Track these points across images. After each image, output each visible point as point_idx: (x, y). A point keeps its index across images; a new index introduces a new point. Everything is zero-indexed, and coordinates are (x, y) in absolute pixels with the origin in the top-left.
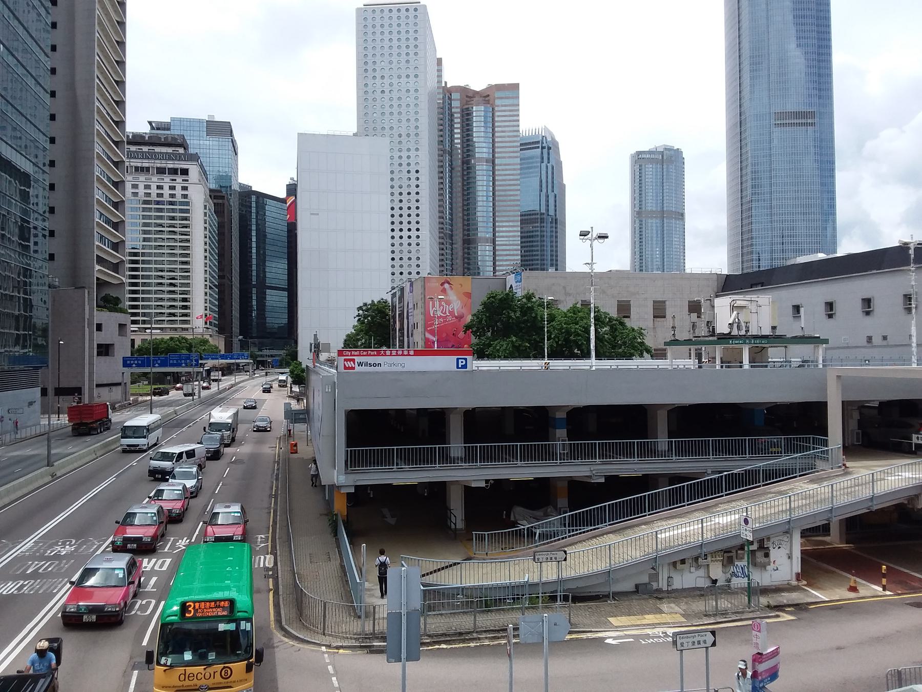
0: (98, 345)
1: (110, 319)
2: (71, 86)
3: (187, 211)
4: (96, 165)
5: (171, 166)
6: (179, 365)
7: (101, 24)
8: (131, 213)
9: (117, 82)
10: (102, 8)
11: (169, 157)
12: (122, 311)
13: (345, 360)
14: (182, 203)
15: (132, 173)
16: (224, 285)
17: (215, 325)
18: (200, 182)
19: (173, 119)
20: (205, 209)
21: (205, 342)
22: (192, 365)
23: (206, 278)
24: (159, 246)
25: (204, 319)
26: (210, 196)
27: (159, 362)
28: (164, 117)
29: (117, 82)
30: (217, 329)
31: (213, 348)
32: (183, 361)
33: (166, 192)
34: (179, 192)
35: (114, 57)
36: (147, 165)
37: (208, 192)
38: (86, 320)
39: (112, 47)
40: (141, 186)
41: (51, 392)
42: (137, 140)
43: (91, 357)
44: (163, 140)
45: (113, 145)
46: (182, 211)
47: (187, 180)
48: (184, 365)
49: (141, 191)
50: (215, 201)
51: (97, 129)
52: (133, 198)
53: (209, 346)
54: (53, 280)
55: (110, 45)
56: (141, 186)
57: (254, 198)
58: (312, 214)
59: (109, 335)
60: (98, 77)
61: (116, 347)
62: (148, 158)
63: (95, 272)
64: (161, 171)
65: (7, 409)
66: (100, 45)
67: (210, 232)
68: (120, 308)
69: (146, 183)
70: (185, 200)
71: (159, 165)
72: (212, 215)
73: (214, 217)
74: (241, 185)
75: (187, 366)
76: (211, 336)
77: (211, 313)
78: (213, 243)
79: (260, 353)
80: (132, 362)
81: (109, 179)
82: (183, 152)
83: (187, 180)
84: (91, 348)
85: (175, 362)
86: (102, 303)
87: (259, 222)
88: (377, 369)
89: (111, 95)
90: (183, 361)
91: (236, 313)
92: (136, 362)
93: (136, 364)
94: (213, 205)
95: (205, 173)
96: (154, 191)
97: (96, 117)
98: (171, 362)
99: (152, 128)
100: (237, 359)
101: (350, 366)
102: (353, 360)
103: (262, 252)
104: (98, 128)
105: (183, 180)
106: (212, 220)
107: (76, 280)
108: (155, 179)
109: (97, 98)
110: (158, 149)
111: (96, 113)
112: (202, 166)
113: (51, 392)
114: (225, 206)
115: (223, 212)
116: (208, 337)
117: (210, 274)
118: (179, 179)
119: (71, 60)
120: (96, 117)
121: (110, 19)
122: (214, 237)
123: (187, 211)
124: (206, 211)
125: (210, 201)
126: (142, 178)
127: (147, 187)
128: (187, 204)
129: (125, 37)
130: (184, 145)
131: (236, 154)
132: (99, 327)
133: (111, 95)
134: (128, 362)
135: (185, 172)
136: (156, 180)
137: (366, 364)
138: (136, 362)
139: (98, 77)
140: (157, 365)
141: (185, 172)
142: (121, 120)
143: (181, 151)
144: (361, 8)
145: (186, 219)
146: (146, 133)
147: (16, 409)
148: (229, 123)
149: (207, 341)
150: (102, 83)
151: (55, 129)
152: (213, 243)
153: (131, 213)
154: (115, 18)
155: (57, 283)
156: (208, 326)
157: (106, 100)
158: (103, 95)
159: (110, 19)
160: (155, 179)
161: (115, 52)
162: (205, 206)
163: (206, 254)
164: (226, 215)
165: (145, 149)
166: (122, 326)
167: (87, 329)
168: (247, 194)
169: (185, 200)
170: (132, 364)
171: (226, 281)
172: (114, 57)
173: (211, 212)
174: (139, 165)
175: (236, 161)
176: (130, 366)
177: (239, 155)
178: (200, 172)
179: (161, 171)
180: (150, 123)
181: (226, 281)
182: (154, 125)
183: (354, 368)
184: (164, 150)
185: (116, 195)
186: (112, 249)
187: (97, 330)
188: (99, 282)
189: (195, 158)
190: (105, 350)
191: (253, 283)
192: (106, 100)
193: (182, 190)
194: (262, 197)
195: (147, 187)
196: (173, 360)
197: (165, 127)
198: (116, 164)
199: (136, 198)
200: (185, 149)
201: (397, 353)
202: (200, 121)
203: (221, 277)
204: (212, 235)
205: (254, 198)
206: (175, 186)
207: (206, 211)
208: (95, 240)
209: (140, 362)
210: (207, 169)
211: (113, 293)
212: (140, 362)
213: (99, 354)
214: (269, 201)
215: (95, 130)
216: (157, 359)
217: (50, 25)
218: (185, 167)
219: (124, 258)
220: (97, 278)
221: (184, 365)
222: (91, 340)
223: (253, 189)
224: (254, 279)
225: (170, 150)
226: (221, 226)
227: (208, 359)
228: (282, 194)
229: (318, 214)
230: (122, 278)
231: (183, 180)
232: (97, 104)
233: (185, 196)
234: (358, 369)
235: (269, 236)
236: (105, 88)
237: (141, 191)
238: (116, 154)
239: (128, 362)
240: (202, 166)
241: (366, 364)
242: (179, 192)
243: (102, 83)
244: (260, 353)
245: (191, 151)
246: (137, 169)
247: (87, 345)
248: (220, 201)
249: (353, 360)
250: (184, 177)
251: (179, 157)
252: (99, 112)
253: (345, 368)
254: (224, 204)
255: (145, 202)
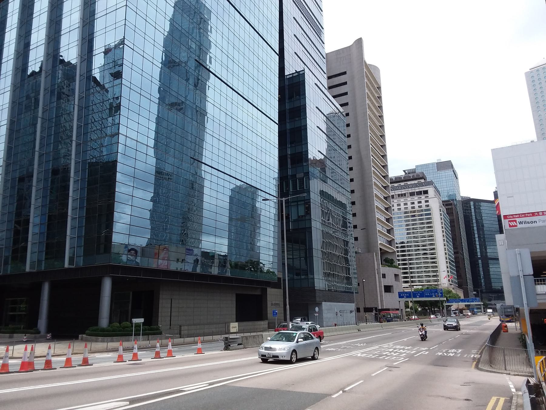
0: (385, 286)
1: (389, 271)
2: (359, 152)
3: (430, 214)
4: (376, 212)
5: (418, 190)
6: (431, 296)
7: (370, 118)
8: (398, 224)
9: (381, 146)
10: (371, 111)
11: (416, 186)
12: (395, 267)
13: (509, 221)
14: (426, 210)
15: (396, 198)
16: (458, 258)
17: (455, 283)
18: (435, 196)
19: (417, 166)
20: (441, 211)
21: (449, 292)
22: (438, 296)
23: (446, 257)
24: (418, 254)
25: (448, 278)
26: (443, 205)
27: (419, 294)
28: (412, 166)
29: (381, 146)
30: (457, 285)
31: (456, 295)
32: (433, 294)
33: (416, 205)
34: (423, 204)
35: (379, 134)
36: (403, 193)
37: (442, 202)
38: (376, 270)
39: (378, 139)
40: (402, 204)
41: (362, 310)
42: (398, 180)
43: (381, 292)
44: (412, 177)
45: (382, 168)
46: (426, 215)
47: (428, 197)
48: (434, 296)
49: (402, 207)
50: (447, 207)
51: (373, 170)
52: (398, 211)
53: (452, 294)
54: (358, 250)
55: (377, 120)
56: (402, 204)
57: (472, 203)
58: (508, 197)
59: (389, 281)
60: (372, 155)
61: (394, 287)
62: (405, 188)
63: (379, 245)
64: (412, 194)
65: (339, 311)
66: (371, 129)
67: (445, 225)
68: (395, 265)
69: (404, 202)
70: (428, 208)
71: (411, 191)
72: (445, 214)
73: (446, 216)
74: (462, 197)
75: (436, 297)
76: (453, 289)
77: (452, 275)
78: (448, 231)
79: (489, 303)
80: (404, 295)
81: (382, 186)
82: (424, 181)
83: (428, 197)
84: (380, 287)
85: (428, 294)
86: (384, 263)
87: (477, 211)
88: (534, 225)
89: (380, 163)
90: (433, 294)
91: (469, 276)
92: (406, 295)
93: (406, 296)
94: (445, 209)
95: (438, 191)
96: (409, 206)
97: (372, 164)
98: (426, 294)
99: (406, 173)
100: (471, 302)
101: (514, 225)
102: (515, 221)
103: (482, 240)
104: (373, 169)
105: (425, 197)
106: (445, 218)
107: (369, 246)
108: (409, 199)
109: (373, 166)
110: (409, 183)
111: (374, 197)
112: (435, 187)
113: (362, 310)
114: (453, 209)
115: (453, 213)
116: (451, 289)
117: (449, 259)
118: (423, 197)
119: (358, 140)
120: (372, 164)
121: (375, 116)
122: (447, 224)
123: (430, 214)
124: (441, 212)
125: (443, 207)
126: (402, 200)
127: (406, 204)
128: (429, 210)
129: (382, 103)
130: (424, 178)
131: (457, 179)
132: (384, 276)
133: (380, 163)
134: (402, 295)
135: (426, 192)
136: (410, 200)
137: (525, 223)
138: (406, 295)
139: (372, 155)
140: (418, 297)
141: (426, 192)
142: (385, 154)
143: (423, 181)
144: (528, 72)
145: (431, 227)
146: (402, 176)
147: (343, 311)
148: (450, 161)
149: (451, 291)
150: (374, 158)
151: (353, 174)
152: (448, 231)
153: (398, 224)
154: (378, 114)
155: (360, 251)
156: (451, 283)
157: (378, 166)
158: (376, 164)
159: (374, 106)
160: (409, 199)
161: (380, 141)
162: (440, 210)
163: (443, 230)
164: (454, 215)
165: (402, 184)
166: (396, 276)
167: (377, 275)
168: (467, 202)
169: (428, 208)
170: (404, 296)
171: (459, 255)
172: (376, 95)
173: (444, 213)
174: (400, 193)
175: (458, 183)
176: (403, 297)
177: (459, 177)
178: (435, 191)
179: (412, 194)
180: (404, 171)
181: (459, 255)
182: (406, 171)
183: (515, 226)
184: (413, 182)
185: (388, 226)
186: (389, 245)
187: (385, 292)
188: (382, 251)
189: (431, 183)
190: (388, 289)
191: (479, 257)
192: (378, 166)
193: (425, 202)
194: (477, 202)
195: (406, 204)
196: (427, 293)
197: (413, 171)
198: (385, 187)
199: (400, 211)
200: (425, 180)
201: (543, 214)
202: (433, 164)
203: (455, 253)
204: (446, 226)
205: (472, 203)
206: (421, 201)
207: (441, 212)
208: (378, 240)
209: (408, 295)
210: (440, 190)
211: (390, 257)
212: (408, 295)
213: (385, 291)
214: (482, 204)
215: (374, 194)
216: (418, 293)
217: (347, 136)
218: (426, 189)
219: (394, 238)
220: (380, 248)
221: (434, 296)
222: (380, 282)
223: (471, 198)
224: (479, 254)
225: (416, 182)
226: (452, 222)
227: (453, 302)
228: (492, 198)
229: (512, 197)
230: (394, 248)
231: (425, 197)
232: (373, 169)
233: (428, 206)
234: (519, 226)
235: (485, 225)
236: (376, 160)
237: (402, 207)
238: (384, 182)
239: (402, 295)
240: (435, 187)
241: (525, 223)
242: (423, 204)
243: (374, 158)
244: (489, 303)
245: (428, 180)
246: (399, 195)
247: (378, 288)
248: (450, 207)
249: (515, 221)
250: (426, 195)
251: (421, 185)
252: (374, 173)
253: (510, 226)
254: (452, 208)
255: (406, 213)
